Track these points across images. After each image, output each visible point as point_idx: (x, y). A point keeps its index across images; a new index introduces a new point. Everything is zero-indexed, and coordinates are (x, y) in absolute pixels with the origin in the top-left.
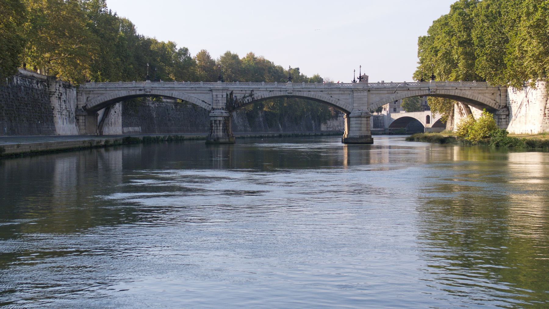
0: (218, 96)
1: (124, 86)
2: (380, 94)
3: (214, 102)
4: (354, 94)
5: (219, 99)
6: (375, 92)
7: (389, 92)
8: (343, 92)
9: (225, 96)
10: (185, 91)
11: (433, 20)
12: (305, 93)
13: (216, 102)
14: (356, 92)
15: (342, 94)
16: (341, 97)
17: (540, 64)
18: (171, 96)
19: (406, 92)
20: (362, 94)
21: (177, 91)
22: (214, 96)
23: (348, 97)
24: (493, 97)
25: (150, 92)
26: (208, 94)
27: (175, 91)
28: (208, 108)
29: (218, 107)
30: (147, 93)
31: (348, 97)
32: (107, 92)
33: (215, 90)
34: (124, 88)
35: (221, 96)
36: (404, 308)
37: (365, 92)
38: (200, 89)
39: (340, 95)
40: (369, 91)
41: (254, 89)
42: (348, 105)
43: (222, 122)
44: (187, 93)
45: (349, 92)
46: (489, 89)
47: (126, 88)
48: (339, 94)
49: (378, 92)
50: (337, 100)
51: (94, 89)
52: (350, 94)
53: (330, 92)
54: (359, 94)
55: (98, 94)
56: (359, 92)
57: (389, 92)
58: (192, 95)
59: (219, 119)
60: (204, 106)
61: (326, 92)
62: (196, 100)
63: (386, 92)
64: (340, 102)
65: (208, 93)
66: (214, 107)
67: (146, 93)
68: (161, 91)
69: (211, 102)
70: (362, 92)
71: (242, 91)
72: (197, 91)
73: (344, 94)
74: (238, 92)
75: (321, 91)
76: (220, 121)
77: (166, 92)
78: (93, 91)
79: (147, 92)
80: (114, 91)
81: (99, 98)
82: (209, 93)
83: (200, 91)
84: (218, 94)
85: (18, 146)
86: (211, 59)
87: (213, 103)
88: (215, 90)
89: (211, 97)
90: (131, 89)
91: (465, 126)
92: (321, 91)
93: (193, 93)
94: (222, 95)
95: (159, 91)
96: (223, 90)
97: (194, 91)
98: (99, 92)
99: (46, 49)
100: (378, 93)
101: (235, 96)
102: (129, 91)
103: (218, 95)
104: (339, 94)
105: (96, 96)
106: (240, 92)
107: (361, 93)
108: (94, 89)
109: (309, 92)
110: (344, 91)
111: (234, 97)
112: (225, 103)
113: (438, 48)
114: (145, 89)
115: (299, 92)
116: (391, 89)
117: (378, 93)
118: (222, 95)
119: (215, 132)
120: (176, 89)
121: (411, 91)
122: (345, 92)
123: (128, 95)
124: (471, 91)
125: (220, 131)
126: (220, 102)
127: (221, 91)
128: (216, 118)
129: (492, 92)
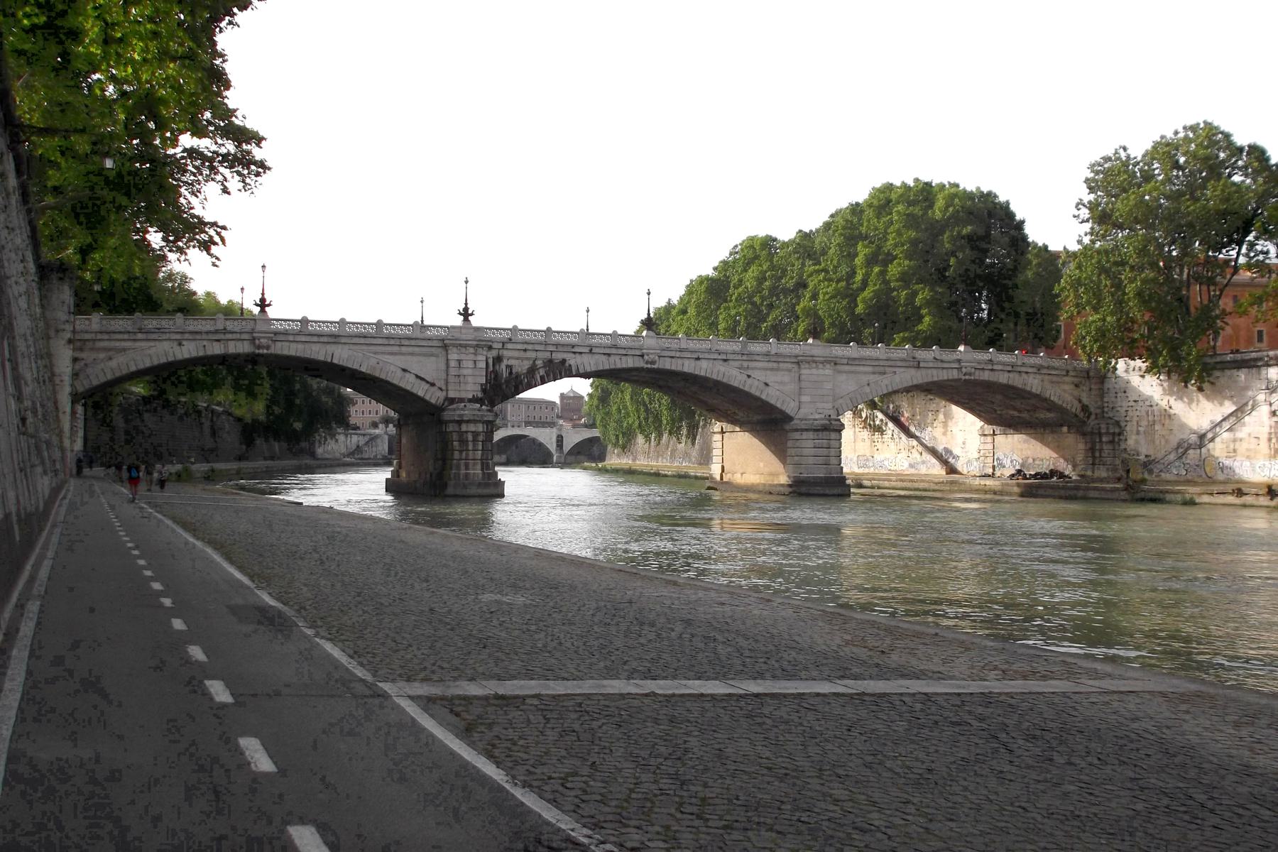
0: (464, 364)
1: (191, 328)
2: (859, 373)
3: (451, 379)
5: (465, 372)
6: (847, 368)
7: (877, 369)
8: (775, 365)
11: (1164, 134)
12: (687, 362)
13: (457, 380)
14: (807, 366)
15: (772, 369)
16: (771, 378)
19: (913, 371)
20: (821, 372)
21: (347, 347)
22: (453, 364)
23: (786, 379)
24: (1076, 393)
25: (268, 347)
26: (433, 359)
27: (340, 346)
28: (434, 397)
29: (463, 395)
30: (261, 351)
31: (786, 379)
32: (138, 344)
33: (454, 346)
34: (191, 333)
35: (471, 364)
36: (2, 383)
37: (828, 366)
38: (413, 343)
39: (769, 372)
40: (835, 364)
42: (788, 399)
43: (481, 438)
44: (375, 353)
45: (790, 366)
47: (197, 333)
48: (766, 369)
49: (853, 368)
50: (762, 386)
51: (99, 337)
52: (789, 371)
53: (745, 364)
54: (814, 371)
55: (110, 350)
56: (814, 365)
57: (877, 369)
58: (390, 359)
59: (472, 428)
61: (737, 364)
62: (399, 373)
63: (870, 369)
64: (770, 390)
66: (452, 394)
67: (257, 351)
68: (300, 346)
69: (443, 382)
70: (821, 366)
71: (525, 350)
73: (778, 369)
74: (516, 354)
75: (725, 360)
76: (476, 434)
77: (315, 348)
78: (94, 340)
79: (259, 347)
80: (157, 343)
81: (113, 363)
82: (437, 356)
84: (463, 357)
87: (447, 383)
88: (454, 346)
89: (443, 367)
90: (211, 337)
91: (1034, 460)
92: (725, 360)
93: (391, 354)
94: (475, 361)
95: (293, 346)
97: (396, 349)
98: (113, 344)
100: (852, 372)
101: (507, 366)
102: (205, 343)
104: (766, 369)
105: (102, 355)
106: (522, 354)
107: (817, 368)
108: (99, 337)
109: (698, 362)
110: (778, 362)
114: (254, 339)
116: (882, 363)
117: (852, 372)
118: (475, 361)
119: (463, 467)
120: (343, 340)
122: (781, 365)
123: (201, 354)
124: (1038, 376)
125: (474, 464)
127: (472, 350)
128: (464, 428)
129: (1076, 380)
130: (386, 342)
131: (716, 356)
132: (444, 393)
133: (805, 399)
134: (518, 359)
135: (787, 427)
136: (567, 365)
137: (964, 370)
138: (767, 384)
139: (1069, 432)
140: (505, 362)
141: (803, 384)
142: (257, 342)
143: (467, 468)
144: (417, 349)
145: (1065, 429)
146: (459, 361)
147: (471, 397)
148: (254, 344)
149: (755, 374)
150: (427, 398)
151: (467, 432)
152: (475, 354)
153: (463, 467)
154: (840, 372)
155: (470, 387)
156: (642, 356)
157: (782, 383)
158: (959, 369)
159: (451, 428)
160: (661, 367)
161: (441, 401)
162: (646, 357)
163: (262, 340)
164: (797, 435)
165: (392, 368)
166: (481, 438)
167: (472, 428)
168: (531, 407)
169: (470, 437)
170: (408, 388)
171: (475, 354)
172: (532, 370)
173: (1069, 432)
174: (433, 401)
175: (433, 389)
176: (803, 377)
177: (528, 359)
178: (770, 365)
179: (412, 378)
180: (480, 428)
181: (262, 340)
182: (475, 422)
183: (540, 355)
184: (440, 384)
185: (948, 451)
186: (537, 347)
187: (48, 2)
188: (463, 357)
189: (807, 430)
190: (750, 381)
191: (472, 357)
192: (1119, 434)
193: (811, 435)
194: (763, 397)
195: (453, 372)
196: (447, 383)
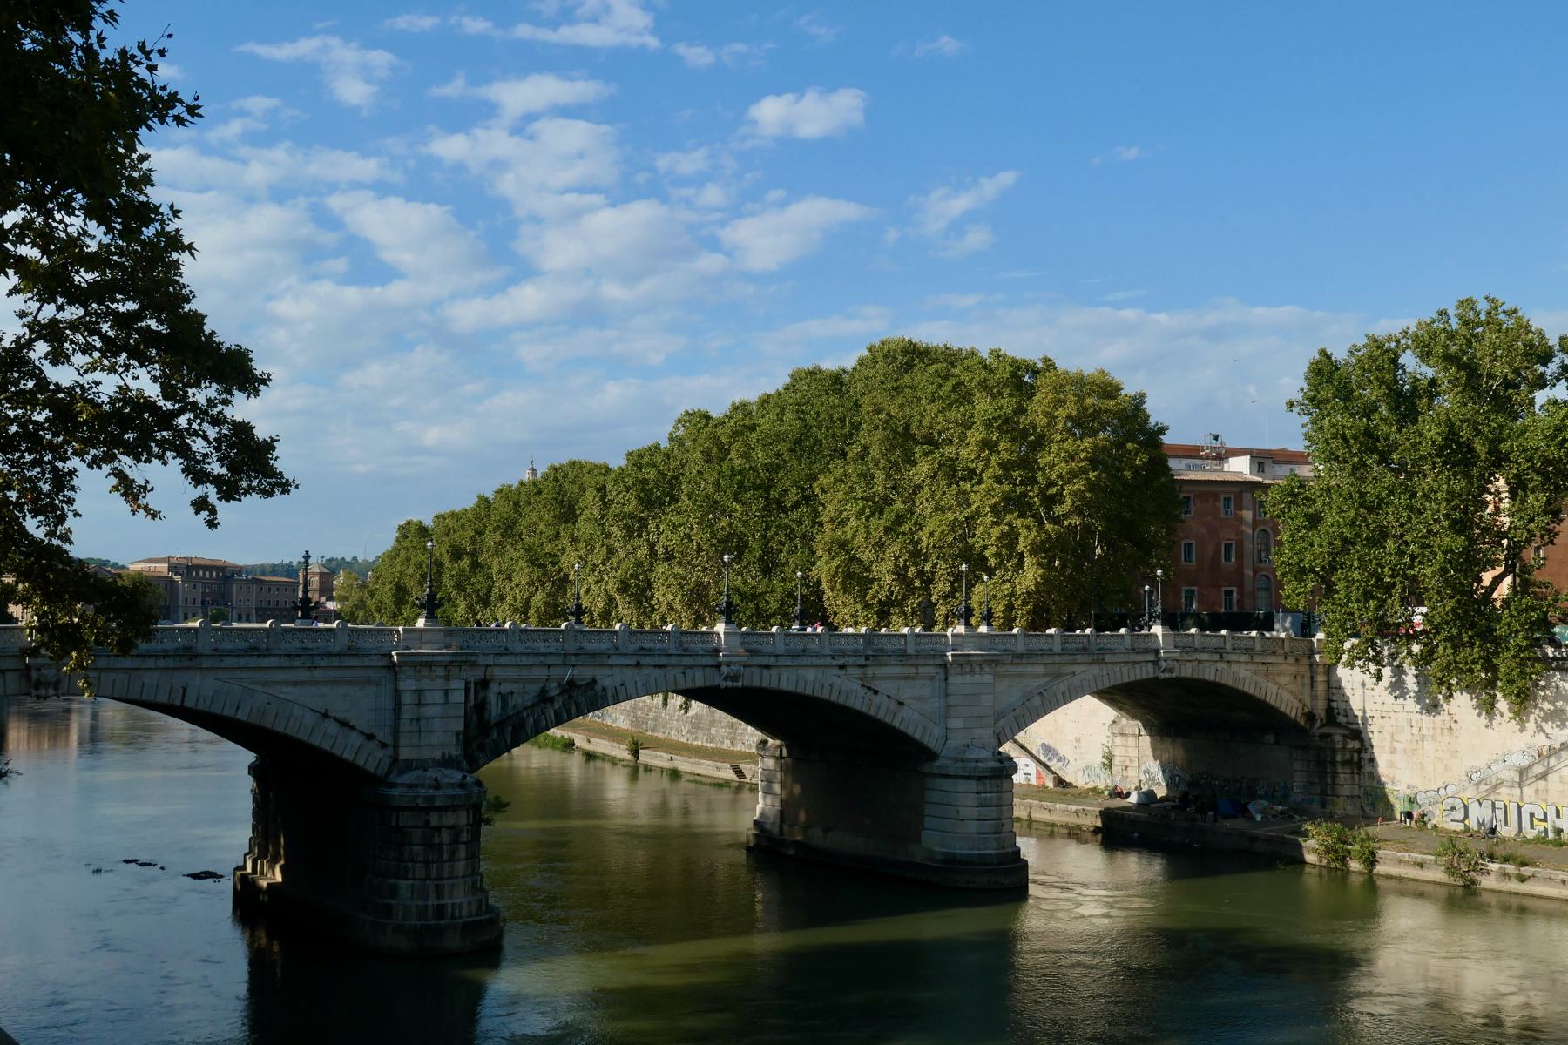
0: (429, 697)
3: (405, 726)
4: (951, 679)
5: (428, 711)
8: (912, 670)
9: (458, 697)
10: (258, 675)
15: (907, 678)
16: (907, 692)
17: (1407, 464)
18: (178, 703)
20: (977, 678)
22: (407, 698)
28: (372, 759)
29: (426, 754)
31: (926, 692)
35: (438, 697)
39: (903, 683)
41: (497, 672)
44: (264, 684)
45: (933, 670)
46: (1226, 657)
50: (893, 706)
52: (932, 678)
58: (291, 692)
60: (348, 748)
62: (310, 719)
64: (905, 711)
65: (368, 682)
66: (405, 754)
72: (317, 673)
74: (512, 673)
75: (842, 667)
76: (455, 830)
82: (378, 684)
83: (331, 674)
85: (719, 769)
86: (226, 346)
92: (842, 667)
93: (296, 684)
94: (446, 692)
96: (448, 666)
99: (1064, 566)
103: (427, 694)
107: (972, 672)
111: (492, 698)
112: (457, 734)
113: (1445, 841)
115: (765, 671)
118: (446, 692)
121: (1110, 667)
122: (921, 670)
124: (1250, 667)
126: (437, 724)
128: (434, 820)
130: (285, 662)
131: (828, 661)
132: (390, 751)
133: (956, 723)
134: (516, 681)
135: (927, 768)
136: (598, 688)
137: (1163, 664)
138: (901, 704)
139: (1277, 743)
140: (494, 688)
141: (953, 701)
142: (34, 675)
143: (440, 895)
144: (339, 673)
145: (1270, 738)
146: (419, 692)
147: (437, 755)
148: (29, 679)
149: (885, 687)
150: (360, 762)
151: (438, 829)
152: (447, 678)
153: (433, 895)
154: (1004, 676)
155: (435, 739)
156: (718, 666)
157: (920, 699)
158: (1156, 663)
159: (406, 820)
160: (747, 683)
161: (385, 765)
162: (724, 669)
163: (44, 671)
164: (947, 784)
165: (297, 711)
166: (465, 837)
167: (450, 819)
168: (265, 588)
169: (446, 837)
170: (326, 746)
171: (447, 678)
172: (544, 698)
173: (1277, 743)
174: (371, 768)
175: (372, 744)
176: (951, 689)
177: (533, 681)
178: (907, 670)
179: (356, 740)
180: (462, 818)
181: (44, 671)
182: (454, 808)
183: (554, 672)
184: (384, 735)
185: (1047, 749)
186: (551, 660)
187: (1565, 427)
188: (425, 684)
189: (968, 778)
190: (876, 699)
191: (440, 683)
192: (1359, 751)
193: (972, 785)
194: (896, 724)
195: (407, 712)
196: (396, 733)
